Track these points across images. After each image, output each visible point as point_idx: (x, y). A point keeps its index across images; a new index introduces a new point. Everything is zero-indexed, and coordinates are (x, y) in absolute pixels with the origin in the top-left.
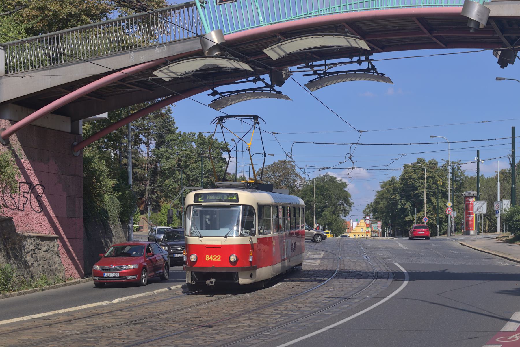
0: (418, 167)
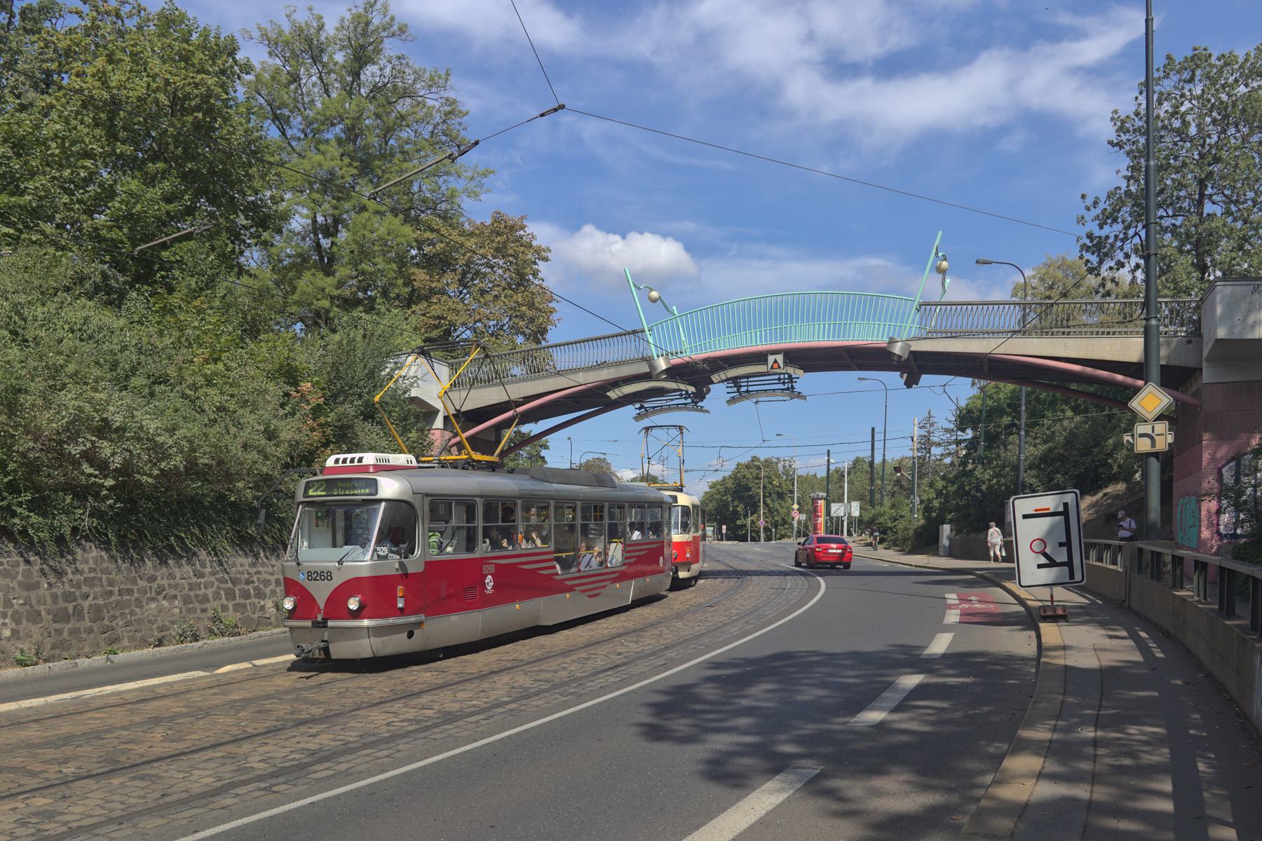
0: (753, 465)
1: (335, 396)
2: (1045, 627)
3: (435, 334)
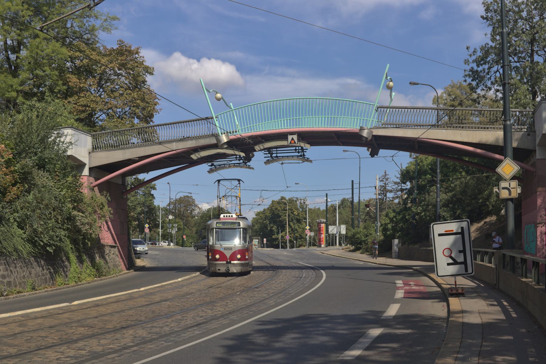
0: (282, 202)
1: (20, 154)
2: (452, 300)
3: (83, 116)
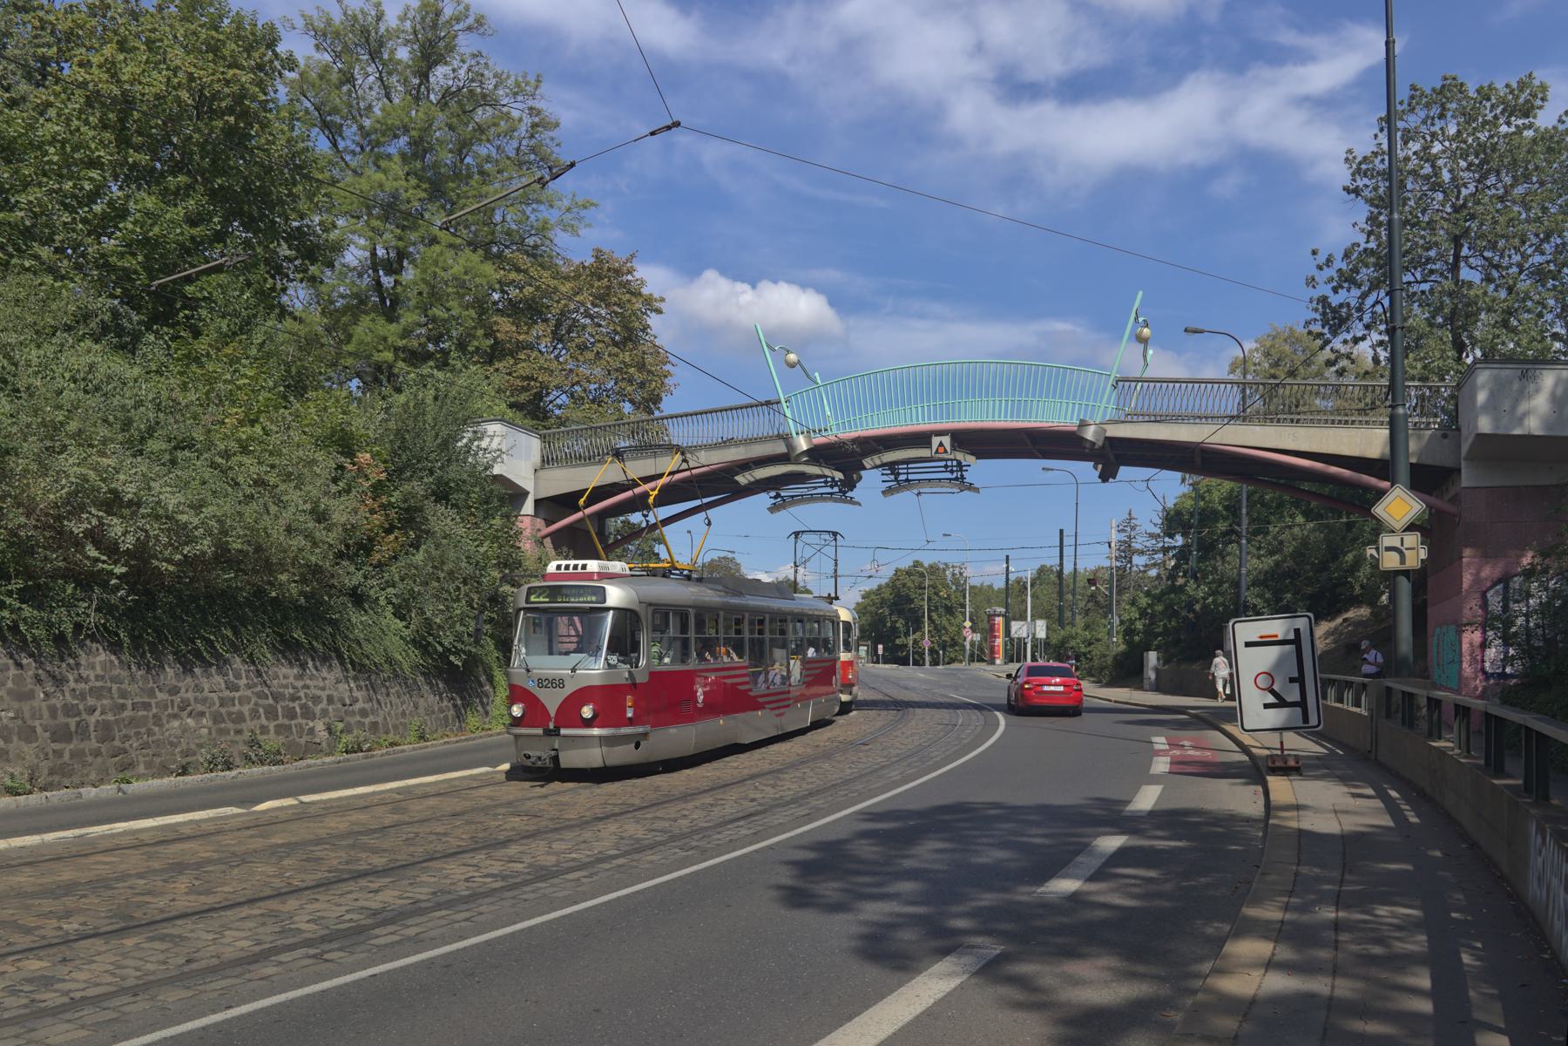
0: (915, 571)
1: (400, 471)
2: (1274, 782)
3: (523, 398)
